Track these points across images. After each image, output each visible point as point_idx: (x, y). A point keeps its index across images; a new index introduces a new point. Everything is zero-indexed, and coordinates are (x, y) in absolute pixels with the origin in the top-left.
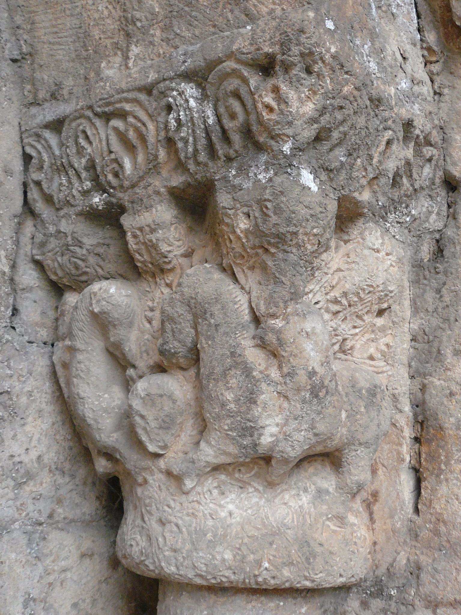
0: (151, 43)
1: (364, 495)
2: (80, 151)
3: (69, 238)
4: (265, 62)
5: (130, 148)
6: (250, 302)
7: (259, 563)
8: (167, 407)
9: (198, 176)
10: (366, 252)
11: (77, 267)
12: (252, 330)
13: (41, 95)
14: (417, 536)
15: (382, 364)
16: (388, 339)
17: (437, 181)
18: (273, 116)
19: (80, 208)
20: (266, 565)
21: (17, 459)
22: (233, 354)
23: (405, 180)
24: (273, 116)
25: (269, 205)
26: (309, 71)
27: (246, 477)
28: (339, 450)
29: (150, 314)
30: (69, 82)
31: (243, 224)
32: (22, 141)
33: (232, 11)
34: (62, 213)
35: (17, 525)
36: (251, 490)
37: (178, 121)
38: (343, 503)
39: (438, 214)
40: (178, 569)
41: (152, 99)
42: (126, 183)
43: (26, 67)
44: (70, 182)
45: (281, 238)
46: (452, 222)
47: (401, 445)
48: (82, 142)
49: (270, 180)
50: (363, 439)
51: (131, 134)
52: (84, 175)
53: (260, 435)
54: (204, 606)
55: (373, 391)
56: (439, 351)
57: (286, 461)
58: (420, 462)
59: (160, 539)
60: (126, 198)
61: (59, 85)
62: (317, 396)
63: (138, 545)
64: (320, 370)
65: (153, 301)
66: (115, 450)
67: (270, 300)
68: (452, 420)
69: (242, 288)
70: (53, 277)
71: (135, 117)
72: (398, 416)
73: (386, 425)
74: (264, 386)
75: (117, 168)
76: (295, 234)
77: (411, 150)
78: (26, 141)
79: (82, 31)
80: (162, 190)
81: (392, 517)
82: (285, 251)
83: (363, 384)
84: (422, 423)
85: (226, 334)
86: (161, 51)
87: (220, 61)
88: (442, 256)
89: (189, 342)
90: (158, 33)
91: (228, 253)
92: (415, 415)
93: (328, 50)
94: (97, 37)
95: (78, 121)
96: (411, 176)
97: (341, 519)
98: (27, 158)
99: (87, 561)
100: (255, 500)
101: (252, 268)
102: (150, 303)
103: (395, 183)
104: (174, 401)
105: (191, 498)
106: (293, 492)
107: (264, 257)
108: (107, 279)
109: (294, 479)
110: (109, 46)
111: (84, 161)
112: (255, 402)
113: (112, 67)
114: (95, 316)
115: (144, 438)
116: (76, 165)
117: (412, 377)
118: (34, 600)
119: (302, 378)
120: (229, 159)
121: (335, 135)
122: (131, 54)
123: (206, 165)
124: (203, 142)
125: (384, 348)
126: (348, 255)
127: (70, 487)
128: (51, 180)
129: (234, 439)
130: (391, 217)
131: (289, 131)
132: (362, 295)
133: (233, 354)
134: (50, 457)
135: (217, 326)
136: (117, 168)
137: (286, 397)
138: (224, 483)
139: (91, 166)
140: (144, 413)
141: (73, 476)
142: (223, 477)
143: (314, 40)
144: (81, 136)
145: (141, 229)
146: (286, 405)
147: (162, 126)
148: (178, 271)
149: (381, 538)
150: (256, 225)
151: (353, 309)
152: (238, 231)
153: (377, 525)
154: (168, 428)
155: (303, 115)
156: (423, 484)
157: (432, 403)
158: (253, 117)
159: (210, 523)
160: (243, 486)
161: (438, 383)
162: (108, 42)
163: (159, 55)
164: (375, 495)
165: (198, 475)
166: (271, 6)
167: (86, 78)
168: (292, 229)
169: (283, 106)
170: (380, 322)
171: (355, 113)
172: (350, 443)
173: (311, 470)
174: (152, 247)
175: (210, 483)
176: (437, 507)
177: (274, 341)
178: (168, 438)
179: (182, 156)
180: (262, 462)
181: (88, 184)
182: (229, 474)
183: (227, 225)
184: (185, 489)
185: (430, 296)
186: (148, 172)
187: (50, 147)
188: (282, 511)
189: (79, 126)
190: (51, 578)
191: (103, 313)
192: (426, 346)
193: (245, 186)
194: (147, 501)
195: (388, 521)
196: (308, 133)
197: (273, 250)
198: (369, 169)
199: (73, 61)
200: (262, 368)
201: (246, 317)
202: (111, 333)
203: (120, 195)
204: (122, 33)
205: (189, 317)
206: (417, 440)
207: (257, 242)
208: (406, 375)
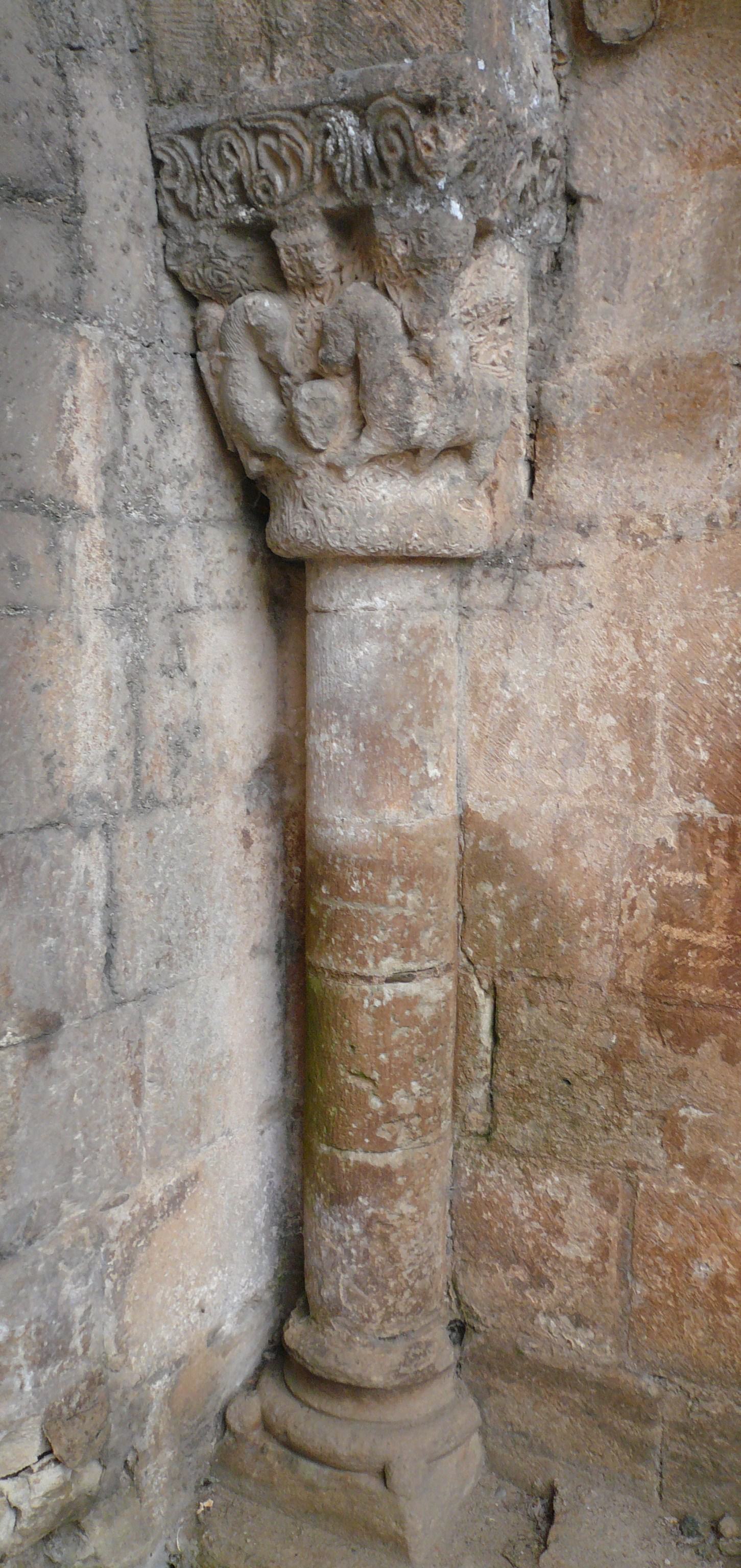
0: (300, 57)
1: (486, 483)
2: (224, 163)
3: (212, 251)
4: (424, 101)
5: (283, 166)
6: (402, 317)
7: (410, 535)
8: (330, 409)
9: (355, 201)
10: (495, 267)
11: (220, 280)
12: (404, 343)
13: (166, 91)
14: (531, 515)
15: (504, 369)
16: (508, 347)
17: (559, 193)
18: (432, 155)
19: (223, 221)
20: (416, 535)
21: (178, 463)
22: (392, 363)
23: (530, 195)
24: (432, 155)
25: (425, 234)
26: (462, 112)
27: (395, 467)
28: (470, 444)
29: (301, 326)
30: (200, 83)
31: (400, 250)
32: (150, 144)
33: (388, 39)
34: (201, 224)
35: (183, 521)
36: (399, 477)
37: (336, 146)
38: (472, 488)
39: (558, 227)
40: (341, 542)
41: (308, 121)
42: (278, 201)
43: (143, 56)
44: (210, 191)
45: (433, 262)
46: (570, 237)
47: (518, 440)
48: (227, 154)
49: (427, 212)
50: (490, 434)
51: (284, 153)
52: (229, 188)
53: (414, 429)
54: (358, 575)
55: (499, 394)
56: (554, 358)
57: (432, 451)
58: (535, 456)
59: (325, 521)
60: (278, 215)
61: (188, 84)
62: (460, 397)
63: (301, 527)
64: (463, 376)
65: (304, 314)
66: (275, 449)
67: (423, 316)
68: (564, 418)
69: (395, 304)
70: (189, 288)
71: (289, 137)
72: (517, 416)
73: (507, 424)
74: (418, 389)
75: (268, 185)
76: (444, 259)
77: (538, 167)
78: (156, 145)
79: (214, 26)
80: (317, 210)
81: (510, 501)
82: (435, 273)
83: (491, 387)
84: (537, 422)
85: (386, 345)
86: (312, 68)
87: (381, 95)
88: (560, 269)
89: (350, 352)
90: (307, 46)
91: (381, 272)
92: (532, 415)
93: (479, 92)
94: (233, 37)
95: (222, 132)
96: (535, 190)
97: (470, 502)
98: (157, 164)
99: (234, 555)
100: (402, 486)
101: (404, 287)
102: (300, 316)
103: (523, 199)
104: (335, 404)
105: (350, 485)
106: (433, 479)
107: (417, 278)
108: (252, 291)
109: (433, 467)
110: (249, 50)
111: (229, 174)
112: (411, 403)
113: (253, 74)
114: (249, 328)
115: (309, 436)
116: (220, 178)
117: (529, 381)
118: (201, 584)
119: (449, 381)
120: (386, 188)
121: (479, 166)
122: (276, 65)
123: (363, 191)
124: (360, 168)
125: (505, 355)
126: (479, 272)
127: (217, 489)
128: (188, 188)
129: (393, 433)
130: (516, 232)
131: (444, 169)
132: (489, 307)
133: (392, 363)
134: (200, 461)
135: (377, 339)
136: (268, 185)
137: (435, 399)
138: (378, 472)
139: (238, 179)
140: (310, 414)
141: (217, 479)
142: (377, 467)
143: (470, 85)
144: (225, 147)
145: (296, 247)
146: (434, 404)
147: (319, 149)
148: (329, 286)
149: (500, 519)
150: (413, 251)
151: (480, 320)
152: (396, 255)
153: (498, 509)
154: (330, 427)
155: (456, 153)
156: (537, 473)
157: (546, 403)
158: (412, 153)
159: (368, 504)
160: (393, 474)
161: (552, 386)
162: (248, 45)
163: (309, 72)
164: (495, 484)
165: (358, 466)
166: (429, 42)
167: (221, 81)
168: (443, 255)
169: (440, 146)
170: (501, 330)
171: (496, 142)
172: (479, 438)
173: (446, 461)
174: (306, 265)
175: (366, 472)
176: (549, 491)
177: (427, 352)
178: (330, 436)
179: (339, 180)
180: (409, 454)
181: (232, 197)
182: (381, 464)
183: (385, 249)
184: (346, 477)
185: (547, 307)
186: (302, 192)
187: (188, 156)
188: (424, 495)
189: (222, 137)
190: (210, 568)
191: (260, 325)
192: (543, 354)
193: (402, 215)
194: (309, 491)
195: (507, 505)
196: (457, 168)
197: (425, 273)
198: (502, 191)
199: (204, 58)
200: (416, 374)
201: (400, 330)
202: (267, 344)
203: (271, 211)
204: (264, 38)
205: (352, 331)
206: (532, 436)
207: (412, 266)
208: (524, 379)
